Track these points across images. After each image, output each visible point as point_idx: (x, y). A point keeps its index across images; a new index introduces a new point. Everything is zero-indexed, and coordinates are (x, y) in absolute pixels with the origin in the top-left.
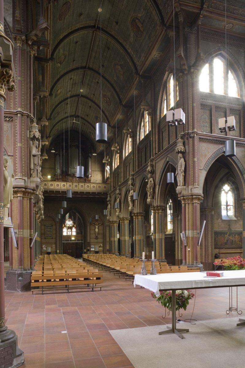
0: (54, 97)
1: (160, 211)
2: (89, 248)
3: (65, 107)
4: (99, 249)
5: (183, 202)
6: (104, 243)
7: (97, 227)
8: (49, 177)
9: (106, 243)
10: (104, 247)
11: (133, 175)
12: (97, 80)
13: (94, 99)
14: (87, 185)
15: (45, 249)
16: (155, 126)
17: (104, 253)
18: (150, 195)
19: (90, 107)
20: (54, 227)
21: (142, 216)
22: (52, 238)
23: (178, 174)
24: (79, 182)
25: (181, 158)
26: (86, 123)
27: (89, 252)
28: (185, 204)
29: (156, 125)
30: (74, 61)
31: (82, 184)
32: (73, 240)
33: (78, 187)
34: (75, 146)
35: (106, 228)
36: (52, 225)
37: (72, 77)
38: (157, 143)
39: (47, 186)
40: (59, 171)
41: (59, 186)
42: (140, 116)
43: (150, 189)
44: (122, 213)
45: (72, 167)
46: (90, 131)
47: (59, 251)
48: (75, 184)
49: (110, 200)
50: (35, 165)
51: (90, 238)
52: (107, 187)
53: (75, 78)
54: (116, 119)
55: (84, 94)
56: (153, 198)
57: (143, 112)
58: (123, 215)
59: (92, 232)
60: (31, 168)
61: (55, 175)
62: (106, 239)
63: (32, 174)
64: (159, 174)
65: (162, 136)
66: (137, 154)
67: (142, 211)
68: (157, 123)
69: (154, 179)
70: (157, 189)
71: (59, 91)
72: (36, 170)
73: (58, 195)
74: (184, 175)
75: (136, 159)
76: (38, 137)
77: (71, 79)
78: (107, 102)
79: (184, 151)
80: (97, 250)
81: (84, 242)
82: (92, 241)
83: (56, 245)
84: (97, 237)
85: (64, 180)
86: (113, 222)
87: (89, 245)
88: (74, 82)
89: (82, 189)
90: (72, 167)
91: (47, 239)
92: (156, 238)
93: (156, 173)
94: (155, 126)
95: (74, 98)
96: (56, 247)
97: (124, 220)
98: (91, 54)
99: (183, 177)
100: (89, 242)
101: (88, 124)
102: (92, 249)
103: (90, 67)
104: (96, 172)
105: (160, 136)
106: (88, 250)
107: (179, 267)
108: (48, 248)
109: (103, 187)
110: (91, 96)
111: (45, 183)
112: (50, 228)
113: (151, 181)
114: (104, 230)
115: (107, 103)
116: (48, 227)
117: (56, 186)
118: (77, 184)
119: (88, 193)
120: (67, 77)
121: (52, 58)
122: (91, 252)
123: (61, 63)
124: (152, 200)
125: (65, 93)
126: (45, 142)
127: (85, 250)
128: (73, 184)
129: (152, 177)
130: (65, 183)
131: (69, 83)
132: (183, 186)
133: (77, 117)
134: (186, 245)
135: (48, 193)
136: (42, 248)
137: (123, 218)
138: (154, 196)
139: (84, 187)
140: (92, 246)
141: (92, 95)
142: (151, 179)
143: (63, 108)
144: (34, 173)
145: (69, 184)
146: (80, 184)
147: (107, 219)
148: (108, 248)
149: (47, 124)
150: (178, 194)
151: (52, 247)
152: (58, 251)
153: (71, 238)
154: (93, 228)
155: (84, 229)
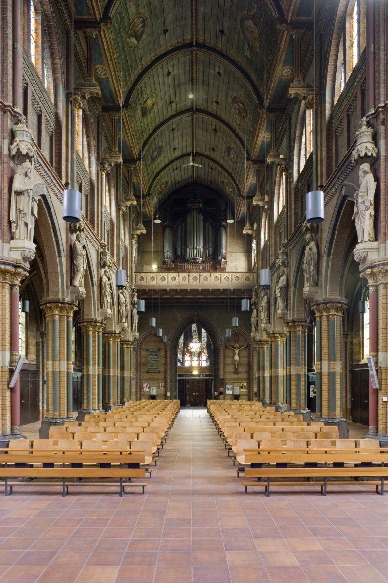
0: (140, 114)
1: (332, 312)
2: (222, 389)
3: (171, 137)
4: (240, 391)
5: (370, 282)
6: (250, 380)
7: (237, 351)
8: (155, 267)
9: (253, 380)
10: (249, 387)
11: (286, 246)
12: (217, 70)
13: (219, 114)
14: (214, 275)
15: (147, 389)
16: (321, 129)
17: (249, 400)
18: (308, 279)
19: (215, 130)
20: (162, 353)
21: (303, 326)
22: (159, 372)
23: (357, 213)
24: (199, 272)
25: (365, 173)
26: (214, 165)
27: (222, 396)
28: (377, 286)
29: (323, 126)
30: (165, 31)
31: (207, 275)
32: (196, 376)
33: (198, 280)
34: (197, 209)
35: (253, 354)
36: (159, 350)
37: (170, 69)
38: (324, 163)
39: (145, 280)
40: (169, 255)
41: (166, 280)
42: (299, 122)
43: (309, 265)
44: (271, 324)
45: (192, 247)
46: (223, 179)
47: (171, 394)
48: (193, 275)
49: (256, 301)
50: (20, 213)
51: (225, 372)
52: (251, 279)
53: (176, 72)
54: (259, 142)
55: (200, 104)
56: (316, 284)
57: (305, 113)
58: (274, 326)
59: (229, 361)
60: (11, 219)
61: (164, 262)
62: (253, 374)
63: (14, 233)
64: (327, 230)
65: (336, 145)
66: (293, 202)
67: (303, 318)
68: (325, 119)
69: (319, 243)
70: (324, 265)
71: (149, 103)
72: (23, 223)
73: (175, 296)
74: (373, 213)
75: (291, 213)
76: (27, 153)
77: (169, 74)
78: (240, 111)
79: (375, 155)
80: (237, 393)
81: (215, 378)
82: (229, 376)
83: (166, 384)
84: (236, 369)
85: (176, 270)
86: (261, 343)
87: (223, 383)
88: (176, 82)
89: (206, 283)
90: (192, 247)
91: (151, 374)
92: (65, 362)
93: (322, 230)
94: (321, 129)
95: (183, 116)
96: (165, 387)
97: (275, 337)
98: (196, 8)
99: (372, 220)
100: (223, 380)
101: (218, 167)
102: (227, 392)
103: (201, 42)
104: (237, 254)
105: (331, 146)
106: (221, 393)
107: (357, 444)
108: (151, 388)
109: (245, 278)
110: (214, 108)
111: (142, 275)
112: (155, 355)
113: (310, 249)
114: (250, 357)
115: (241, 115)
116: (153, 352)
117: (159, 280)
118: (196, 276)
119: (216, 291)
120: (160, 70)
121: (106, 18)
122: (226, 398)
123: (138, 38)
124: (313, 288)
125: (164, 108)
126: (131, 200)
127: (216, 394)
128: (189, 276)
129: (313, 240)
130: (175, 275)
131: (166, 83)
132: (370, 241)
133: (196, 155)
134: (377, 387)
135: (147, 293)
136: (142, 388)
137: (274, 334)
138: (318, 279)
139: (209, 280)
140: (228, 386)
141: (215, 104)
142: (312, 244)
143: (168, 139)
144: (17, 231)
145: (182, 275)
146: (202, 276)
147: (250, 336)
148: (256, 389)
149: (119, 161)
150: (359, 264)
151: (158, 388)
152: (169, 394)
153: (192, 372)
154: (231, 354)
155: (214, 356)
